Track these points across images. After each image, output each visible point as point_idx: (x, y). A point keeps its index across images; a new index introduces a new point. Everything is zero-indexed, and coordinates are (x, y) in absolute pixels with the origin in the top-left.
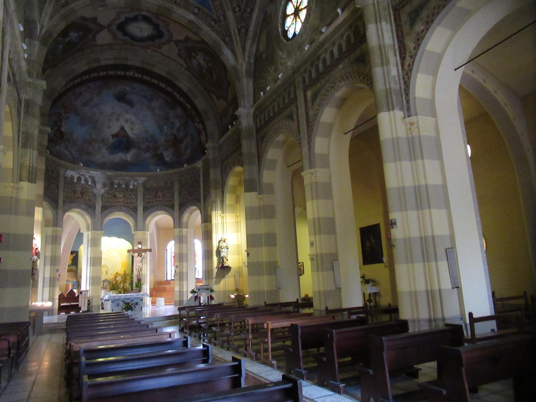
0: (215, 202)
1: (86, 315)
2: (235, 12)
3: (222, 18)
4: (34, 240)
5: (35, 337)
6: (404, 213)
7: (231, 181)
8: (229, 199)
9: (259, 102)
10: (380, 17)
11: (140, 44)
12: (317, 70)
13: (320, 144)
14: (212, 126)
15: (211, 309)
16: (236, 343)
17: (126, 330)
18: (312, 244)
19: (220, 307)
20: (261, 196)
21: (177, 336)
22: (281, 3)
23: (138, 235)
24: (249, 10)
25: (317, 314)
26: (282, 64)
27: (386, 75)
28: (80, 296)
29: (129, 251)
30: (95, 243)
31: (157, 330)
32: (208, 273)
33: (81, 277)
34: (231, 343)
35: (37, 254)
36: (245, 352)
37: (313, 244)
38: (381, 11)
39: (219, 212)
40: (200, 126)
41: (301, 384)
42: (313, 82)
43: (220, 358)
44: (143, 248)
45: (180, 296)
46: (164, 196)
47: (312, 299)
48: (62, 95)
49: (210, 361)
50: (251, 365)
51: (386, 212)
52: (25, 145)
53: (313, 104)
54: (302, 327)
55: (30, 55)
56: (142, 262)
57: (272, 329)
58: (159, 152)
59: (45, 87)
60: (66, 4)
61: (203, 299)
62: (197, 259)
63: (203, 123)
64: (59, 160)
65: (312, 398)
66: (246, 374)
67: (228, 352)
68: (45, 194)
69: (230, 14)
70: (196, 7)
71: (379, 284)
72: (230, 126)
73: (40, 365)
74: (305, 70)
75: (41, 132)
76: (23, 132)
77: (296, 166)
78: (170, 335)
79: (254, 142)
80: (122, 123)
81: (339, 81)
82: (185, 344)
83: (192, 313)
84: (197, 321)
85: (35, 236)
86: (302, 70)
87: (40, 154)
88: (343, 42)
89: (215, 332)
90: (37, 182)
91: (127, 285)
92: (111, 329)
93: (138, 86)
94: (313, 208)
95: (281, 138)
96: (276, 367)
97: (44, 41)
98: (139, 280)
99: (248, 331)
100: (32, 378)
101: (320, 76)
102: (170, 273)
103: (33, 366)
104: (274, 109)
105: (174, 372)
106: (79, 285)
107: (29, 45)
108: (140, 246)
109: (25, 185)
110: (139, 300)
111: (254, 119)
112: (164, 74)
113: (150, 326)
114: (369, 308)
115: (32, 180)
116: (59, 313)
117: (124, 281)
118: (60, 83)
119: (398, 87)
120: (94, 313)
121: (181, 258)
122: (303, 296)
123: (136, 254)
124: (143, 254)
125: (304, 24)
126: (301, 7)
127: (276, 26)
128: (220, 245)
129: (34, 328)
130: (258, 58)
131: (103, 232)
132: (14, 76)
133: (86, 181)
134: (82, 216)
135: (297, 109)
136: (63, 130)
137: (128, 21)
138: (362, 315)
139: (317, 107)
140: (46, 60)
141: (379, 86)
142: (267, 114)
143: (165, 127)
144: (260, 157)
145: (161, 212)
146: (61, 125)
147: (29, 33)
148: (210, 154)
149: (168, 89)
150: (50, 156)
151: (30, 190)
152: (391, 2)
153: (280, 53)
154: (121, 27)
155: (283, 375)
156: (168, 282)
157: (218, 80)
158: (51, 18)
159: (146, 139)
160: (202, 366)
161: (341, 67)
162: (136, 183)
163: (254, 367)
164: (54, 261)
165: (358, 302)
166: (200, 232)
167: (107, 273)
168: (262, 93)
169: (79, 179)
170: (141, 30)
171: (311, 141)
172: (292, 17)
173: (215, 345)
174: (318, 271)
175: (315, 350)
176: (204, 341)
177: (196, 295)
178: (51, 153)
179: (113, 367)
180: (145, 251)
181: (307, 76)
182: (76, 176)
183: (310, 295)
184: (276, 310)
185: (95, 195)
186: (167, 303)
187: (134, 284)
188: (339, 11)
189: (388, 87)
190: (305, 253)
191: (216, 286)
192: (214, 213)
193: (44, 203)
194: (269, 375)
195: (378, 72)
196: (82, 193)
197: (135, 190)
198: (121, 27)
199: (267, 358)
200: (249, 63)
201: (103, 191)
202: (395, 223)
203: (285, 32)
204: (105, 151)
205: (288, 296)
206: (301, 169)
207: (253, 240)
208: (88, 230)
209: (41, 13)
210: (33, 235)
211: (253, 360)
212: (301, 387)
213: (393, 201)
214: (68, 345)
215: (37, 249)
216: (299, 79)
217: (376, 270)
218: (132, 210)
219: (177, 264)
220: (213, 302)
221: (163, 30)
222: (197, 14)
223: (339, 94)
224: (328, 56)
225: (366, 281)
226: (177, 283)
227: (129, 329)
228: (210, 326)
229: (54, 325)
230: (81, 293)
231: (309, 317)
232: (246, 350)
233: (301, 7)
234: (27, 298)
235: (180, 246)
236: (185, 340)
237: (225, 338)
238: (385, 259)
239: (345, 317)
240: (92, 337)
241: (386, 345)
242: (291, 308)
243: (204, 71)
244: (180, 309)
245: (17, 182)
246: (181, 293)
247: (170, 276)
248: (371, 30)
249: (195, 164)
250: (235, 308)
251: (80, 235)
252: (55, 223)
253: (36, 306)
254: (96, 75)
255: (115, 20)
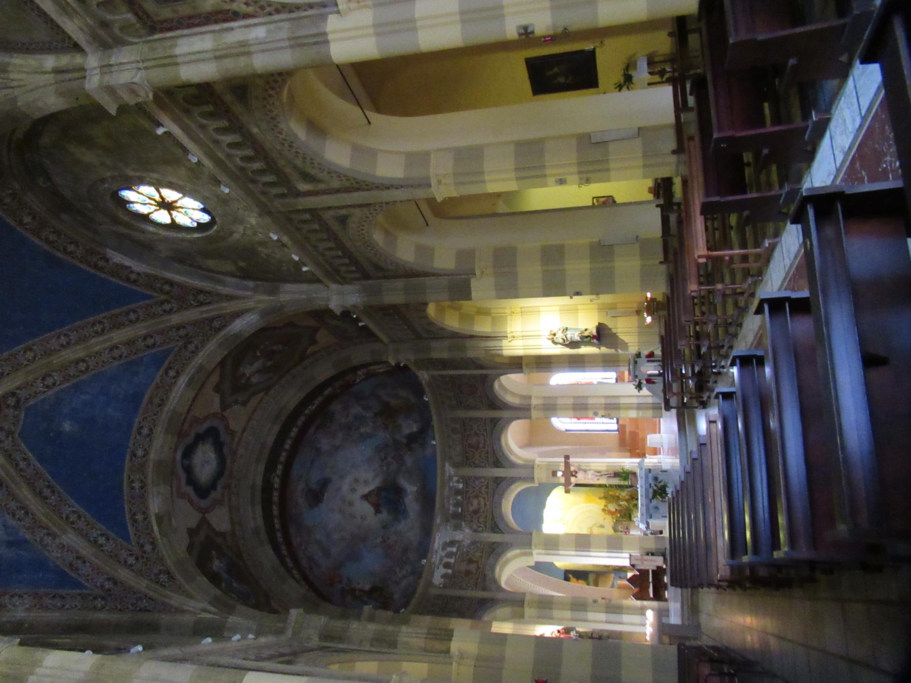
0: (487, 350)
1: (671, 557)
2: (171, 310)
3: (182, 332)
4: (546, 635)
5: (705, 637)
6: (506, 11)
7: (452, 322)
8: (482, 327)
9: (319, 274)
10: (165, 57)
11: (228, 461)
12: (262, 172)
13: (389, 169)
14: (360, 354)
15: (669, 356)
16: (730, 310)
17: (699, 498)
18: (561, 182)
19: (667, 342)
20: (478, 272)
21: (714, 412)
22: (153, 233)
23: (540, 476)
24: (167, 288)
25: (683, 170)
26: (255, 233)
27: (265, 47)
28: (639, 568)
29: (567, 491)
30: (553, 543)
31: (701, 444)
32: (607, 363)
33: (608, 566)
34: (730, 320)
35: (567, 631)
36: (746, 295)
37: (561, 180)
38: (157, 56)
39: (505, 343)
40: (360, 373)
41: (808, 190)
42: (283, 179)
43: (755, 337)
44: (563, 468)
45: (647, 408)
46: (476, 434)
47: (656, 179)
48: (311, 585)
49: (759, 353)
50: (769, 283)
51: (504, 46)
52: (393, 644)
53: (320, 181)
54: (707, 195)
55: (249, 631)
56: (585, 471)
57: (708, 249)
58: (404, 441)
59: (301, 610)
60: (168, 573)
61: (652, 370)
62: (584, 381)
63: (355, 369)
64: (417, 596)
65: (834, 170)
66: (785, 290)
67: (745, 326)
68: (471, 617)
69: (175, 319)
70: (166, 373)
71: (634, 55)
72: (360, 324)
73: (750, 629)
74: (264, 193)
75: (371, 619)
76: (372, 645)
77: (424, 207)
78: (711, 422)
79: (386, 284)
80: (356, 497)
81: (280, 133)
82: (727, 396)
83: (675, 387)
84: (690, 378)
85: (538, 634)
86: (263, 199)
87: (406, 622)
88: (213, 124)
89: (709, 348)
90: (451, 627)
91: (624, 494)
92: (696, 517)
93: (296, 470)
94: (498, 181)
95: (378, 237)
96: (776, 240)
97: (231, 610)
98: (616, 475)
99: (710, 292)
100: (773, 641)
101: (272, 167)
102: (606, 425)
103: (751, 640)
104: (330, 249)
105: (776, 413)
106: (620, 570)
107: (234, 631)
108: (560, 474)
109: (455, 646)
110: (650, 475)
111: (346, 283)
112: (277, 428)
113: (695, 456)
114: (676, 74)
115: (448, 635)
116: (666, 600)
117: (617, 499)
118: (293, 588)
119: (286, 25)
120: (668, 547)
121: (580, 406)
122: (651, 197)
123: (573, 479)
124: (572, 469)
125: (185, 192)
126: (157, 198)
127: (192, 242)
128: (561, 341)
129: (687, 638)
130: (245, 275)
131: (534, 532)
132: (282, 655)
133: (450, 555)
134: (507, 561)
135: (330, 208)
136: (367, 587)
137: (191, 481)
138: (688, 86)
139: (325, 173)
140: (257, 606)
141: (284, 59)
142: (338, 261)
143: (362, 430)
144: (410, 274)
145: (503, 444)
146: (360, 590)
147: (217, 631)
148: (405, 357)
149: (299, 423)
150: (410, 608)
151: (464, 638)
152: (140, 37)
153: (236, 236)
154: (203, 491)
155: (792, 223)
156: (621, 429)
157: (283, 342)
158: (192, 597)
159: (383, 461)
160: (768, 371)
161: (255, 130)
162: (455, 479)
163: (774, 276)
164: (579, 606)
165: (665, 94)
166: (537, 376)
167: (602, 526)
168: (305, 269)
169: (447, 565)
170: (205, 461)
171: (382, 185)
172: (174, 213)
173: (731, 347)
174: (608, 170)
175: (748, 171)
176: (723, 367)
177: (644, 382)
178: (405, 605)
179: (762, 525)
180: (567, 465)
181: (274, 191)
182: (442, 571)
183: (650, 183)
184: (674, 243)
185: (473, 543)
186: (656, 430)
187: (622, 483)
188: (160, 131)
189: (287, 44)
190: (577, 194)
191: (630, 348)
192: (507, 352)
193: (486, 619)
194: (788, 251)
195: (261, 62)
196: (470, 561)
197: (466, 480)
198: (203, 491)
199: (758, 257)
200: (255, 290)
201: (467, 531)
202: (525, 28)
203: (201, 227)
204: (402, 526)
205: (651, 222)
206: (431, 201)
207: (553, 287)
208: (531, 554)
209: (183, 612)
210: (536, 636)
211: (762, 280)
212: (814, 189)
213: (485, 34)
214: (721, 583)
215: (559, 632)
216: (278, 204)
217: (608, 63)
218: (499, 485)
219: (591, 414)
220: (658, 352)
221: (205, 426)
222: (178, 373)
223: (300, 132)
224: (239, 153)
225: (627, 81)
226: (623, 414)
227: (698, 486)
228: (699, 356)
229: (685, 607)
230: (633, 566)
231: (690, 184)
232: (742, 294)
233: (157, 198)
234: (639, 647)
235: (561, 409)
236: (721, 396)
237: (720, 330)
238: (588, 46)
239: (690, 118)
240: (708, 547)
241: (744, 36)
242: (673, 218)
243: (270, 363)
244: (668, 407)
245: (451, 657)
246: (639, 407)
247: (611, 425)
248: (191, 73)
249: (424, 383)
250: (669, 314)
251: (539, 567)
252: (517, 604)
253: (652, 635)
254: (279, 534)
255: (191, 503)
